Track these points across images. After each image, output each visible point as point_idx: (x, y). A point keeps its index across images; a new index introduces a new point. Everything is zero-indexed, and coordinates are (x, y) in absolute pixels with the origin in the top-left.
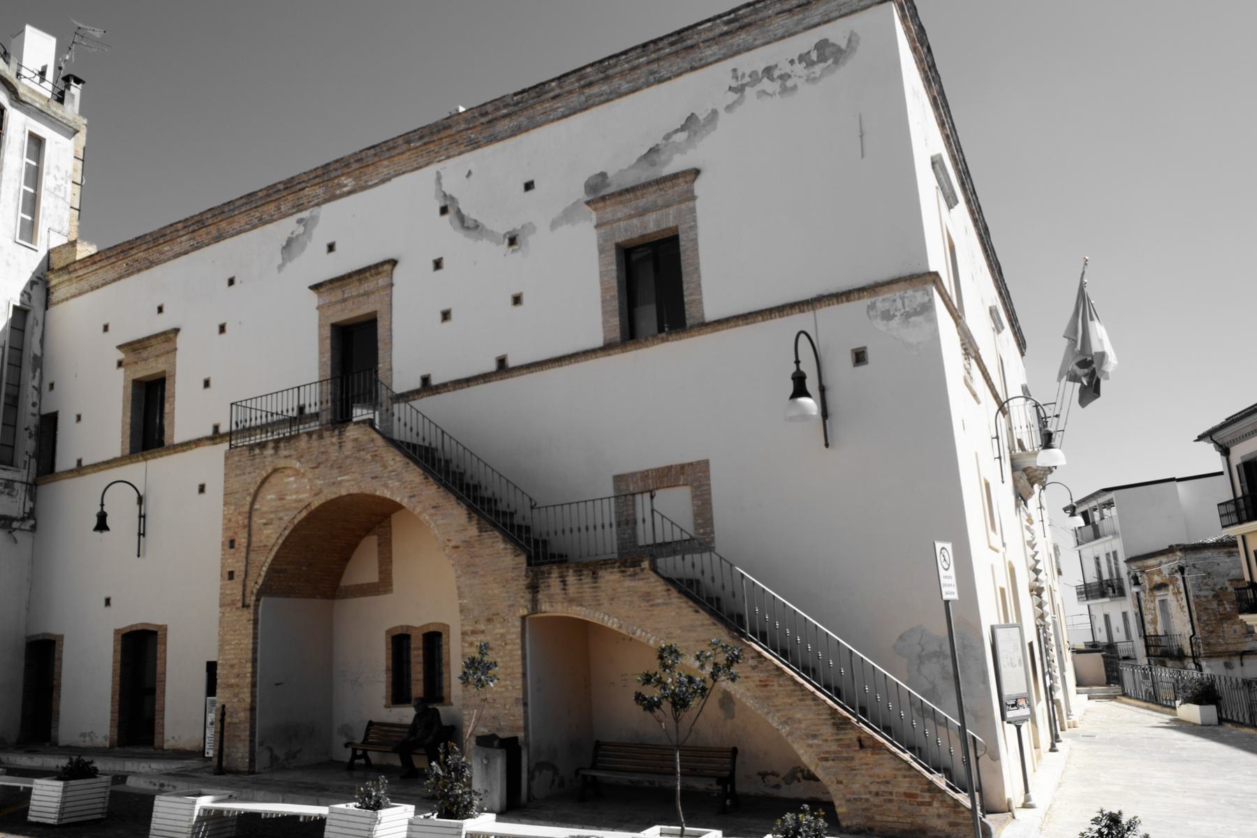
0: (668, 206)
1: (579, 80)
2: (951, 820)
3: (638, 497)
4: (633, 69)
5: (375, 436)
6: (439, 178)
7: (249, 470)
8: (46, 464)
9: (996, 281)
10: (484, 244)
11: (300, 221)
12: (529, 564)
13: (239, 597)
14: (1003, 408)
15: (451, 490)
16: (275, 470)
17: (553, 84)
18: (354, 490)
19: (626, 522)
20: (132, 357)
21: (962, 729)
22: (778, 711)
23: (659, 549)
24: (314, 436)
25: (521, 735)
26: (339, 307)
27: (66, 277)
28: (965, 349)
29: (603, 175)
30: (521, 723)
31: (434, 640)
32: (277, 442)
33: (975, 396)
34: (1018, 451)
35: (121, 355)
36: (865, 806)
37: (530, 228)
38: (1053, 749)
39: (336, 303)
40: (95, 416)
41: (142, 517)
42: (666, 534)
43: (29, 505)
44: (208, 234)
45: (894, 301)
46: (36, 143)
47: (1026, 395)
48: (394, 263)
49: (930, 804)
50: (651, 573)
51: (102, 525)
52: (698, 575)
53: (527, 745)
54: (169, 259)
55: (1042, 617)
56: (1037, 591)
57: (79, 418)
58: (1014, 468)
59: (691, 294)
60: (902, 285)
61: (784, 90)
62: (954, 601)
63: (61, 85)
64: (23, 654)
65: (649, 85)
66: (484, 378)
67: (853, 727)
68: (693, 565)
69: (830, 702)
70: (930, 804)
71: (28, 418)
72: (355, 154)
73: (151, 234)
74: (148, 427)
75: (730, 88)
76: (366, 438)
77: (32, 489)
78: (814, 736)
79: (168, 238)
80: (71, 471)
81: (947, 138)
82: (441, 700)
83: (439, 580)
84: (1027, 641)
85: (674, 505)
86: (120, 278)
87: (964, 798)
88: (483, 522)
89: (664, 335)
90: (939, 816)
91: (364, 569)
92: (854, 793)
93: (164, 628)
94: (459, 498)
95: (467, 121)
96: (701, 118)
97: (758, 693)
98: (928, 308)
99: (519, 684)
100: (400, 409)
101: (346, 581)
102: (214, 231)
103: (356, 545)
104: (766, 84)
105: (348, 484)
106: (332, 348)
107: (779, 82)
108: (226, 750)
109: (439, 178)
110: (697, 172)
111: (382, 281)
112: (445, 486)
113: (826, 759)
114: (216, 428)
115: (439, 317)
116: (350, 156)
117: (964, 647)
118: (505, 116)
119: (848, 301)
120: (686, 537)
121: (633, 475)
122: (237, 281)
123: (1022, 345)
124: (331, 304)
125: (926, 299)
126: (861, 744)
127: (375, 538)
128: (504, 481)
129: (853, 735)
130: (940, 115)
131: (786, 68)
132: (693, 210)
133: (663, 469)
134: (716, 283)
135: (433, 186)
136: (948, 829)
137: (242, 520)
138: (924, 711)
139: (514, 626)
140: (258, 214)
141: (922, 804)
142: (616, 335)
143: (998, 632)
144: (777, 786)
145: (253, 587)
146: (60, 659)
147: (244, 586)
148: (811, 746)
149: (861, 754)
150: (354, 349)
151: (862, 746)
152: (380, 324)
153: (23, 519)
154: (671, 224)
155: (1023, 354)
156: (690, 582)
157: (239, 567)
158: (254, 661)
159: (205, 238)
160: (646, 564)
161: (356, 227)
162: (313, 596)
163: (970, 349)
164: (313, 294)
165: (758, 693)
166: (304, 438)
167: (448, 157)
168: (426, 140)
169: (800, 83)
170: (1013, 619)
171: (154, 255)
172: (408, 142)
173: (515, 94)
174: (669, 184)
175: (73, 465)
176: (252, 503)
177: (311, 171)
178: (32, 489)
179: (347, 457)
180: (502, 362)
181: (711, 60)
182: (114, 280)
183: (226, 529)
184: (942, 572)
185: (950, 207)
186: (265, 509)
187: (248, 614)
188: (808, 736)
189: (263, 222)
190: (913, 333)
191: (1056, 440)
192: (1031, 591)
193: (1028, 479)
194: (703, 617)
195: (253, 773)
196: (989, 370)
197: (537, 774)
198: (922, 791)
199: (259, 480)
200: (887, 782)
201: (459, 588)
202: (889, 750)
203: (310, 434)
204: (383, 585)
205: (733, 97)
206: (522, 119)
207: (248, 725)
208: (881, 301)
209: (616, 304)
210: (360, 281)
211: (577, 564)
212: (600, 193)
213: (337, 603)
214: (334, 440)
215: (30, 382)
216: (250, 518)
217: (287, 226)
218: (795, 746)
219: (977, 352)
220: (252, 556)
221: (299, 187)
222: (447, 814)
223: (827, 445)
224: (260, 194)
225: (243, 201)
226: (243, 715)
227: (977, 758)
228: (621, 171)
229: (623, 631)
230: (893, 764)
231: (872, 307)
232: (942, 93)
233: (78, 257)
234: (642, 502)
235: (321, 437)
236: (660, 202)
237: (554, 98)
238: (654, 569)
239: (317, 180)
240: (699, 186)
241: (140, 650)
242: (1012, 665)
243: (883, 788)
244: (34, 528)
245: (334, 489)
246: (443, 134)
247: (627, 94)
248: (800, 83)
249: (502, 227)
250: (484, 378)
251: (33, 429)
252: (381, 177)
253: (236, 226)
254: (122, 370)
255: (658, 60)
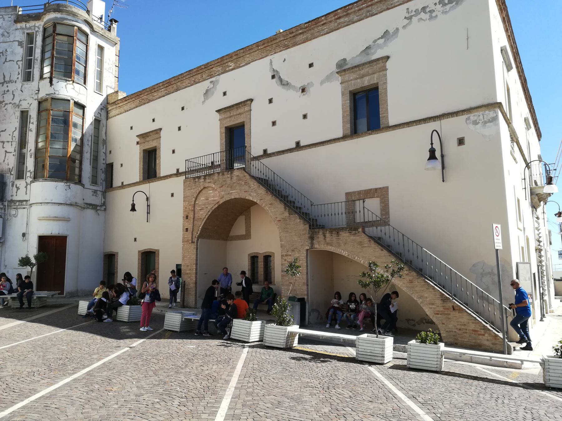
0: (374, 74)
1: (334, 16)
2: (493, 342)
3: (357, 202)
4: (360, 10)
5: (246, 174)
6: (271, 62)
7: (193, 187)
8: (109, 184)
9: (528, 105)
10: (291, 92)
11: (211, 82)
12: (310, 228)
13: (190, 239)
14: (528, 166)
15: (278, 197)
16: (204, 188)
17: (323, 18)
18: (237, 197)
19: (351, 212)
20: (143, 140)
21: (501, 305)
22: (417, 293)
23: (365, 224)
24: (220, 174)
25: (306, 297)
26: (228, 119)
27: (115, 107)
28: (512, 138)
29: (345, 60)
30: (306, 292)
31: (267, 258)
32: (205, 176)
33: (515, 160)
34: (534, 185)
35: (138, 140)
36: (455, 334)
37: (311, 84)
38: (541, 320)
39: (227, 118)
40: (128, 167)
41: (148, 206)
42: (370, 217)
43: (103, 200)
44: (172, 88)
45: (479, 116)
46: (101, 48)
47: (540, 159)
48: (252, 100)
49: (484, 335)
50: (363, 234)
51: (133, 209)
52: (383, 236)
53: (308, 301)
54: (157, 99)
55: (541, 262)
56: (539, 250)
57: (122, 165)
58: (532, 194)
59: (383, 114)
60: (483, 109)
61: (431, 18)
62: (500, 250)
63: (109, 23)
64: (103, 259)
65: (367, 17)
66: (290, 150)
67: (451, 301)
68: (381, 231)
69: (441, 290)
70: (484, 335)
71: (102, 166)
72: (235, 52)
73: (149, 88)
74: (150, 171)
75: (405, 18)
76: (242, 175)
77: (104, 193)
78: (433, 304)
79: (156, 90)
80: (120, 187)
81: (509, 37)
82: (271, 283)
83: (270, 236)
84: (533, 272)
85: (373, 205)
86: (136, 107)
87: (501, 335)
88: (291, 210)
89: (370, 132)
90: (488, 340)
91: (239, 228)
92: (449, 329)
93: (158, 251)
94: (281, 201)
95: (284, 36)
96: (391, 32)
97: (408, 285)
98: (495, 119)
99: (305, 277)
100: (255, 163)
101: (232, 234)
102: (175, 86)
103: (236, 219)
104: (422, 15)
105: (235, 194)
106: (226, 137)
107: (429, 14)
108: (185, 299)
109: (271, 62)
110: (388, 57)
111: (246, 108)
112: (275, 195)
113: (438, 314)
114: (178, 170)
115: (271, 124)
116: (232, 53)
117: (503, 271)
118: (300, 34)
119: (457, 116)
120: (378, 219)
121: (354, 192)
122: (185, 108)
123: (539, 135)
124: (225, 118)
125: (495, 115)
126: (454, 308)
127: (244, 216)
128: (300, 194)
129: (450, 305)
130: (506, 26)
131: (432, 7)
132: (385, 75)
133: (368, 190)
134: (395, 109)
135: (269, 66)
136: (491, 346)
137: (191, 208)
138: (483, 298)
139: (303, 253)
140: (193, 79)
141: (480, 335)
142: (348, 132)
143: (520, 265)
144: (414, 325)
145: (196, 235)
146: (117, 262)
147: (192, 234)
148: (431, 308)
149: (454, 313)
150: (235, 137)
151: (454, 309)
152: (246, 127)
153: (101, 206)
154: (375, 82)
155: (539, 140)
156: (379, 238)
157: (190, 227)
158: (196, 264)
159: (172, 90)
160: (360, 230)
161: (236, 84)
162: (219, 239)
163: (514, 138)
164: (217, 114)
165: (408, 285)
166: (216, 175)
167: (275, 53)
168: (266, 45)
169: (439, 14)
170: (526, 260)
171: (150, 97)
172: (258, 46)
173: (306, 23)
174: (375, 63)
175: (120, 185)
176: (195, 201)
177: (216, 60)
178: (104, 193)
179: (234, 183)
180: (298, 143)
181: (397, 4)
182: (134, 108)
183: (184, 211)
184: (495, 237)
185: (508, 71)
186: (200, 203)
187: (194, 246)
188: (430, 304)
189: (196, 83)
190: (488, 130)
191: (554, 181)
192: (536, 250)
193: (538, 199)
194: (385, 252)
195: (196, 308)
196: (523, 148)
197: (312, 314)
198: (481, 329)
199: (198, 192)
200: (465, 325)
201: (280, 237)
202: (466, 312)
203: (218, 173)
204: (247, 236)
205: (406, 21)
206: (308, 35)
207: (194, 289)
208: (473, 116)
209: (349, 118)
210: (237, 108)
211: (330, 229)
212: (343, 68)
213: (228, 242)
214: (229, 176)
215: (102, 150)
216: (194, 207)
217: (206, 84)
218: (424, 308)
219: (517, 139)
220: (195, 222)
221: (211, 67)
222: (280, 324)
223: (443, 181)
224: (194, 70)
225: (187, 73)
226: (192, 285)
227: (507, 317)
228: (353, 58)
229: (350, 257)
230: (468, 317)
231: (468, 119)
232: (507, 15)
233: (119, 98)
234: (359, 205)
235: (223, 174)
236: (370, 72)
237: (323, 25)
238: (364, 232)
239: (218, 64)
240: (389, 64)
241: (148, 258)
242: (526, 280)
243: (463, 327)
244: (105, 210)
245: (229, 196)
246: (273, 42)
247: (356, 22)
248: (439, 14)
249: (299, 85)
250: (290, 150)
251: (104, 170)
252: (246, 62)
253: (184, 84)
254: (139, 146)
255: (372, 5)
